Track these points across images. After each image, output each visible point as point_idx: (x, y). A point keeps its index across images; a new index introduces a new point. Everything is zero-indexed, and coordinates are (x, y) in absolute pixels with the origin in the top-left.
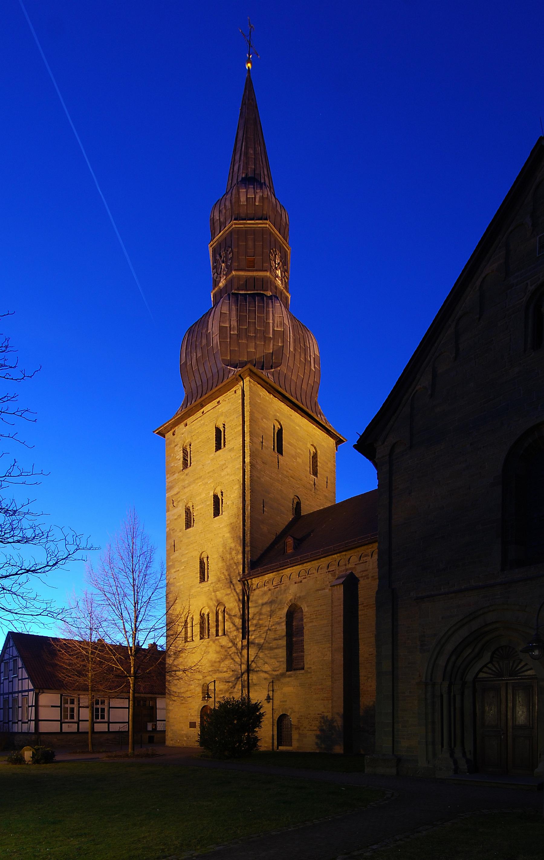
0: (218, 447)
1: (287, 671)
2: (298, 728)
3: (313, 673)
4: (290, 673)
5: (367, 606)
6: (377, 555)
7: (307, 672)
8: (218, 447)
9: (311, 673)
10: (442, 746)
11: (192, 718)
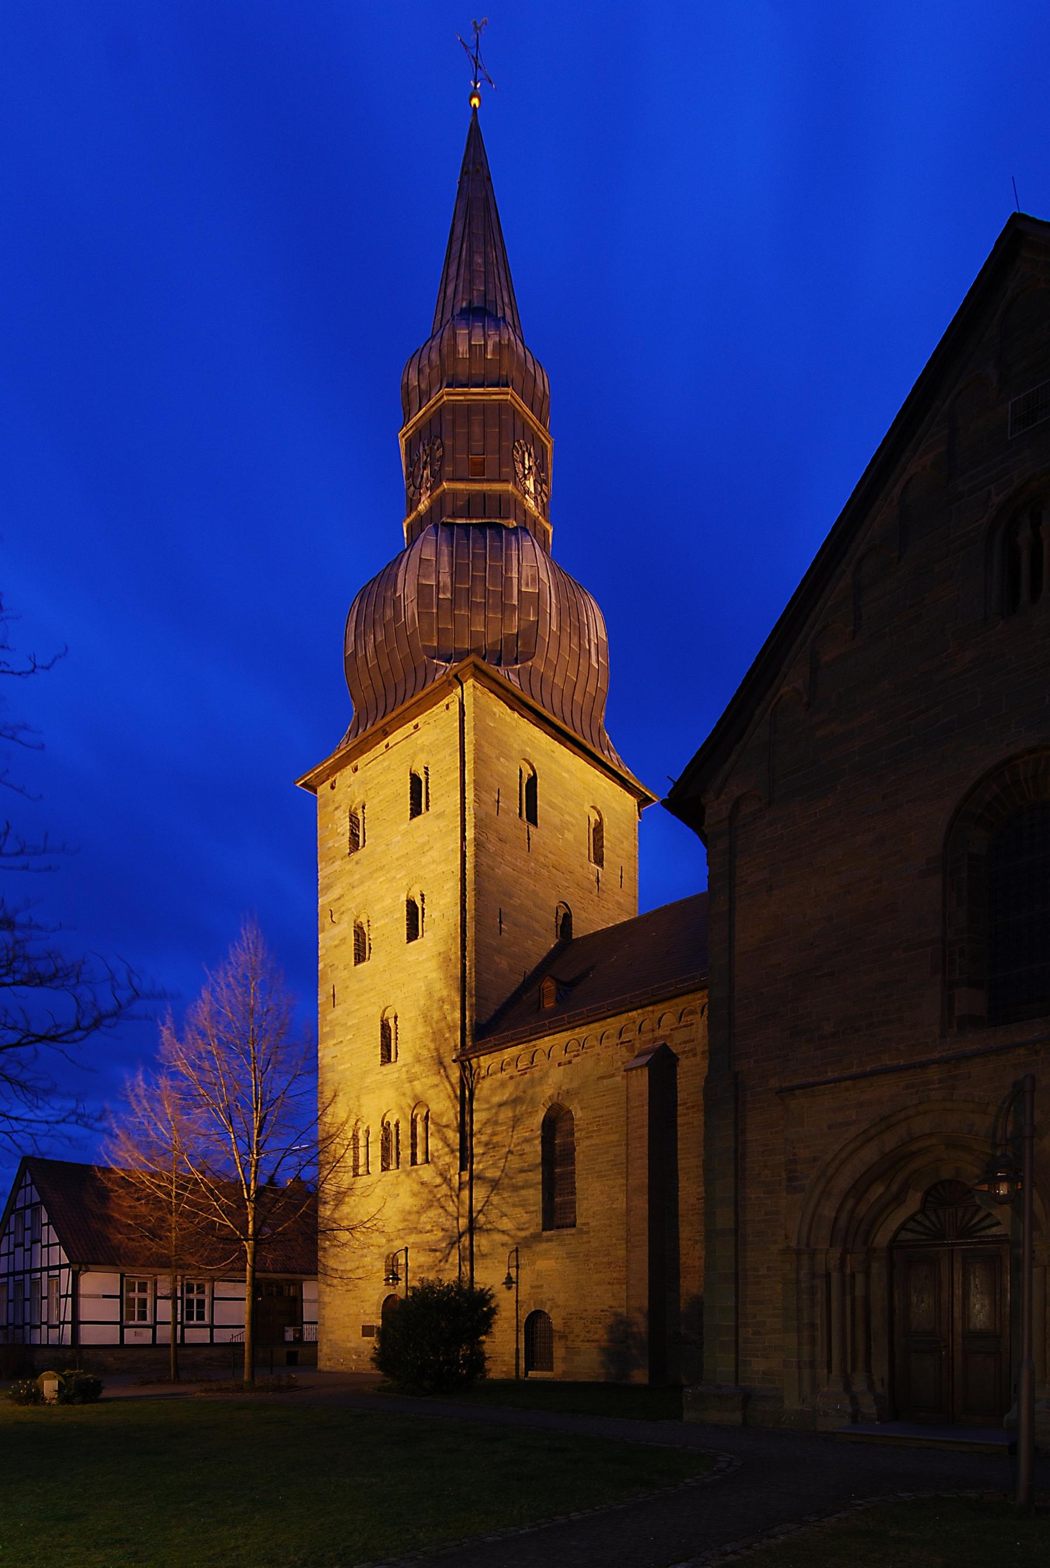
2: (564, 1337)
3: (592, 1234)
5: (693, 1107)
7: (581, 1232)
8: (416, 811)
9: (588, 1233)
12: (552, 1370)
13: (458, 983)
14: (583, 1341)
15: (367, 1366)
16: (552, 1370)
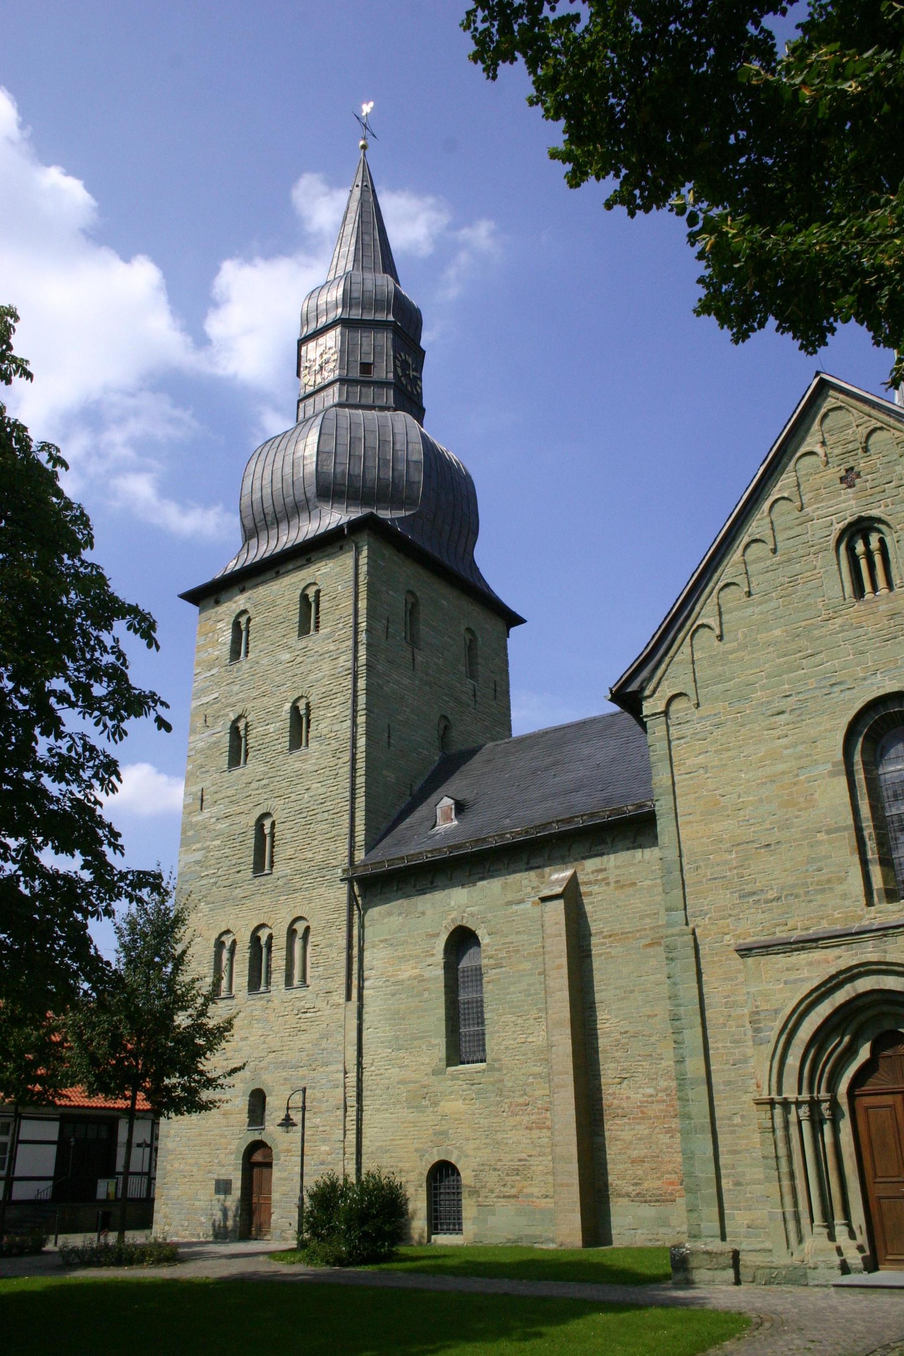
0: (304, 630)
1: (448, 1065)
2: (475, 1192)
3: (505, 1072)
4: (454, 1068)
5: (610, 936)
6: (365, 600)
7: (491, 1069)
8: (304, 630)
9: (500, 1070)
10: (812, 1221)
11: (223, 1171)
12: (459, 1231)
13: (862, 929)
14: (498, 1197)
15: (99, 1181)
16: (459, 1231)
